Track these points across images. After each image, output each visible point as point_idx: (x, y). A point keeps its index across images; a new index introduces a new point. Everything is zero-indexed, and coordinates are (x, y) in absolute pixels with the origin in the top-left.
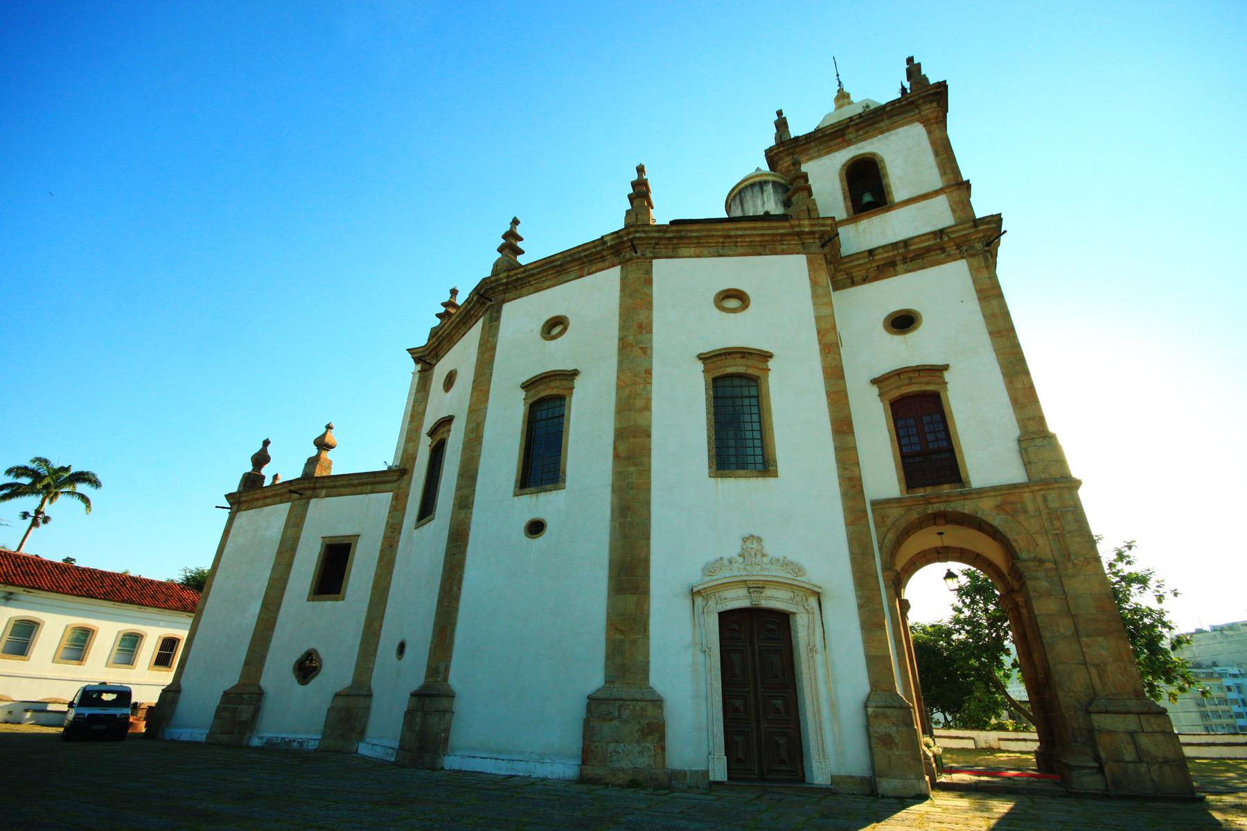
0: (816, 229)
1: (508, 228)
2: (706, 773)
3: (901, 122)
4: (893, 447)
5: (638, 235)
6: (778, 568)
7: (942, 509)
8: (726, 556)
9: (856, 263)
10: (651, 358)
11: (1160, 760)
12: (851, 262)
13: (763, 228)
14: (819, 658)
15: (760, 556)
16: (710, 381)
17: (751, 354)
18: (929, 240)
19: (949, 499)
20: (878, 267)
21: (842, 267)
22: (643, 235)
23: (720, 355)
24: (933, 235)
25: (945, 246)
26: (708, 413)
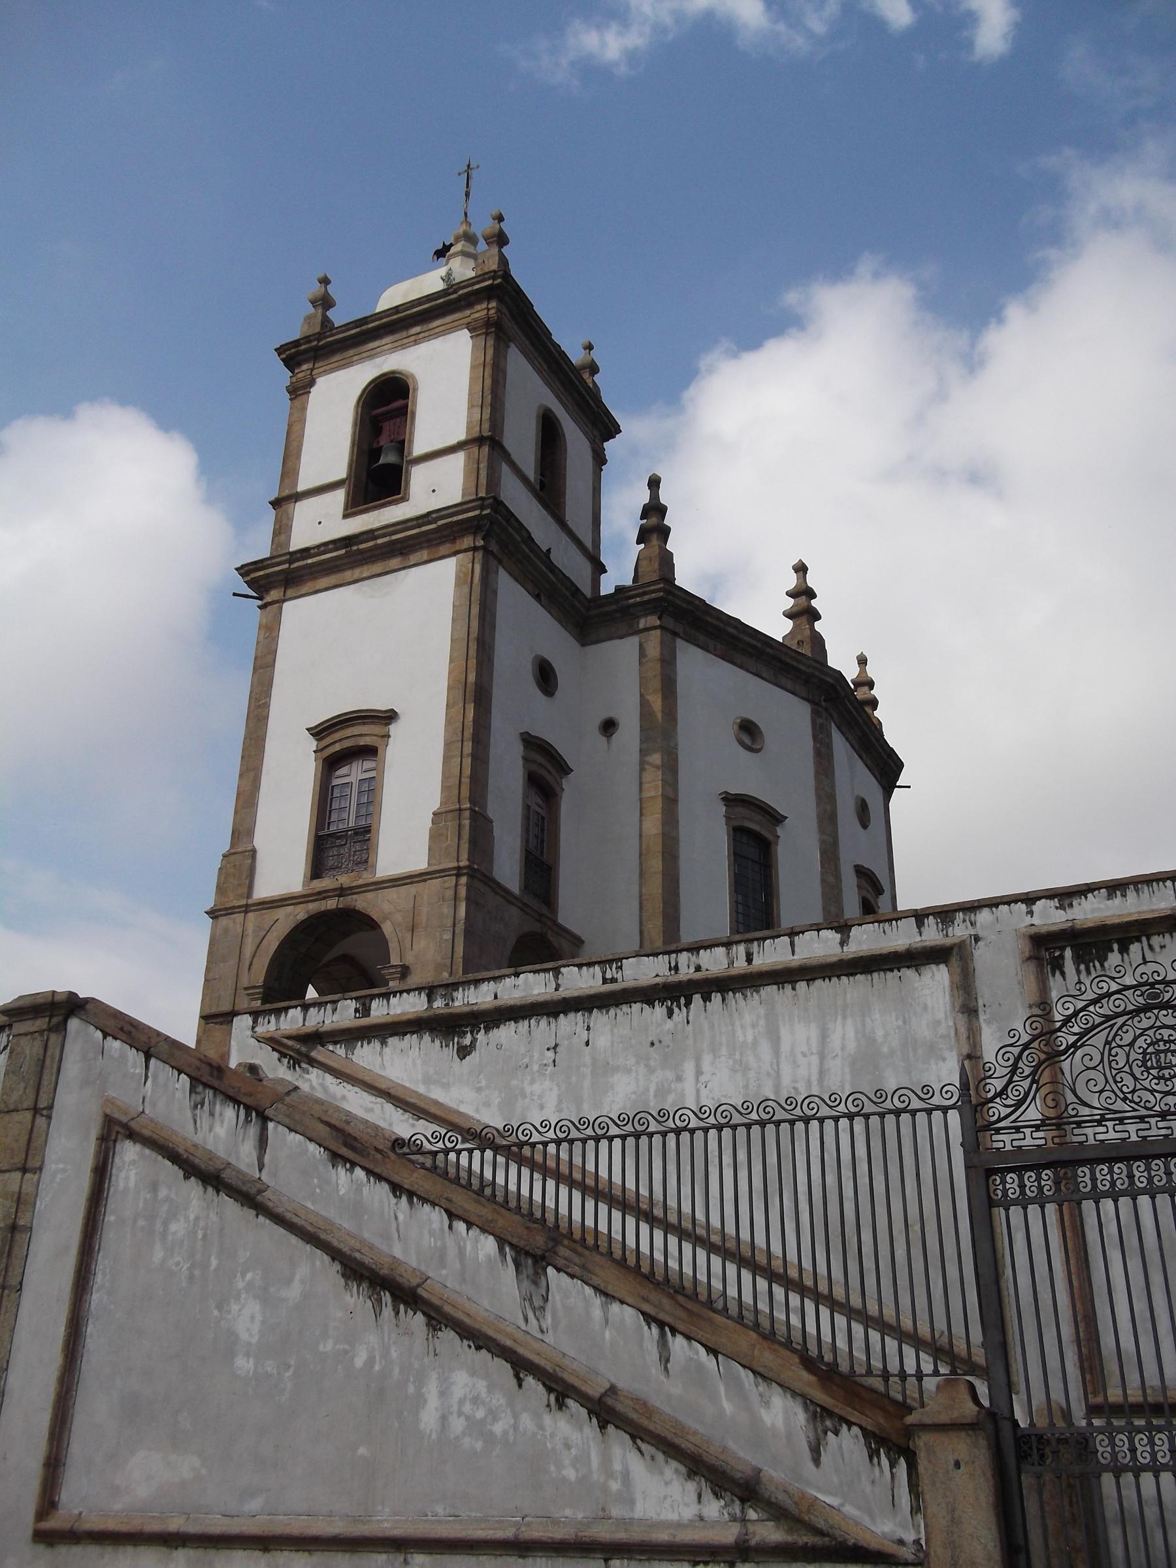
19: (344, 893)
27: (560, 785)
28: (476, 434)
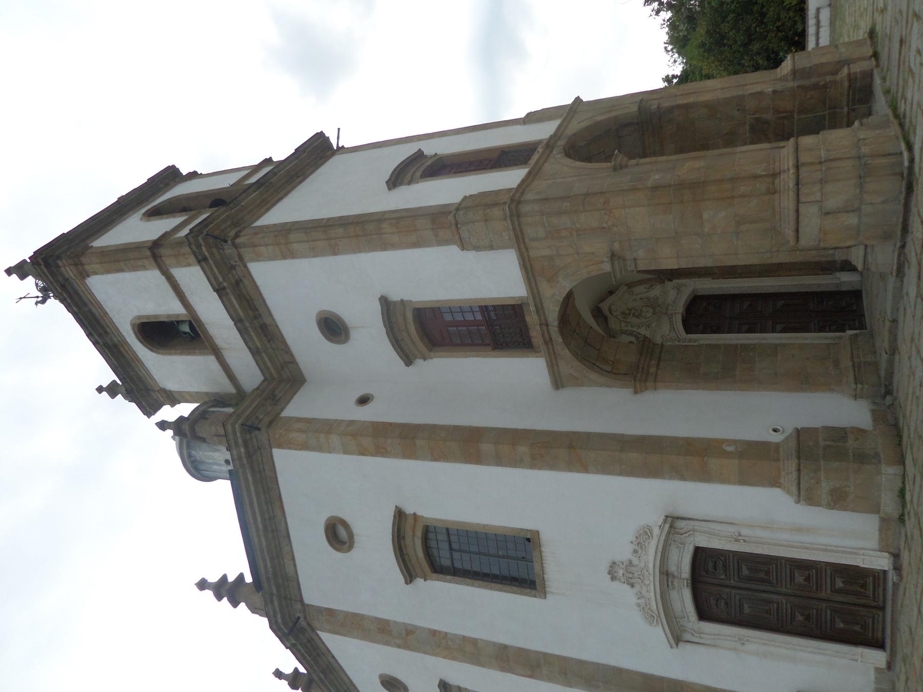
0: (240, 441)
1: (284, 683)
2: (878, 670)
3: (88, 296)
4: (478, 174)
5: (280, 621)
6: (644, 552)
7: (556, 329)
8: (634, 600)
9: (269, 364)
10: (416, 627)
11: (858, 191)
12: (268, 369)
13: (250, 496)
14: (745, 532)
15: (633, 568)
16: (435, 575)
17: (399, 530)
18: (229, 300)
19: (544, 322)
20: (269, 341)
21: (276, 376)
22: (279, 616)
23: (404, 561)
24: (224, 298)
25: (233, 281)
26: (473, 585)
27: (432, 157)
28: (152, 261)
